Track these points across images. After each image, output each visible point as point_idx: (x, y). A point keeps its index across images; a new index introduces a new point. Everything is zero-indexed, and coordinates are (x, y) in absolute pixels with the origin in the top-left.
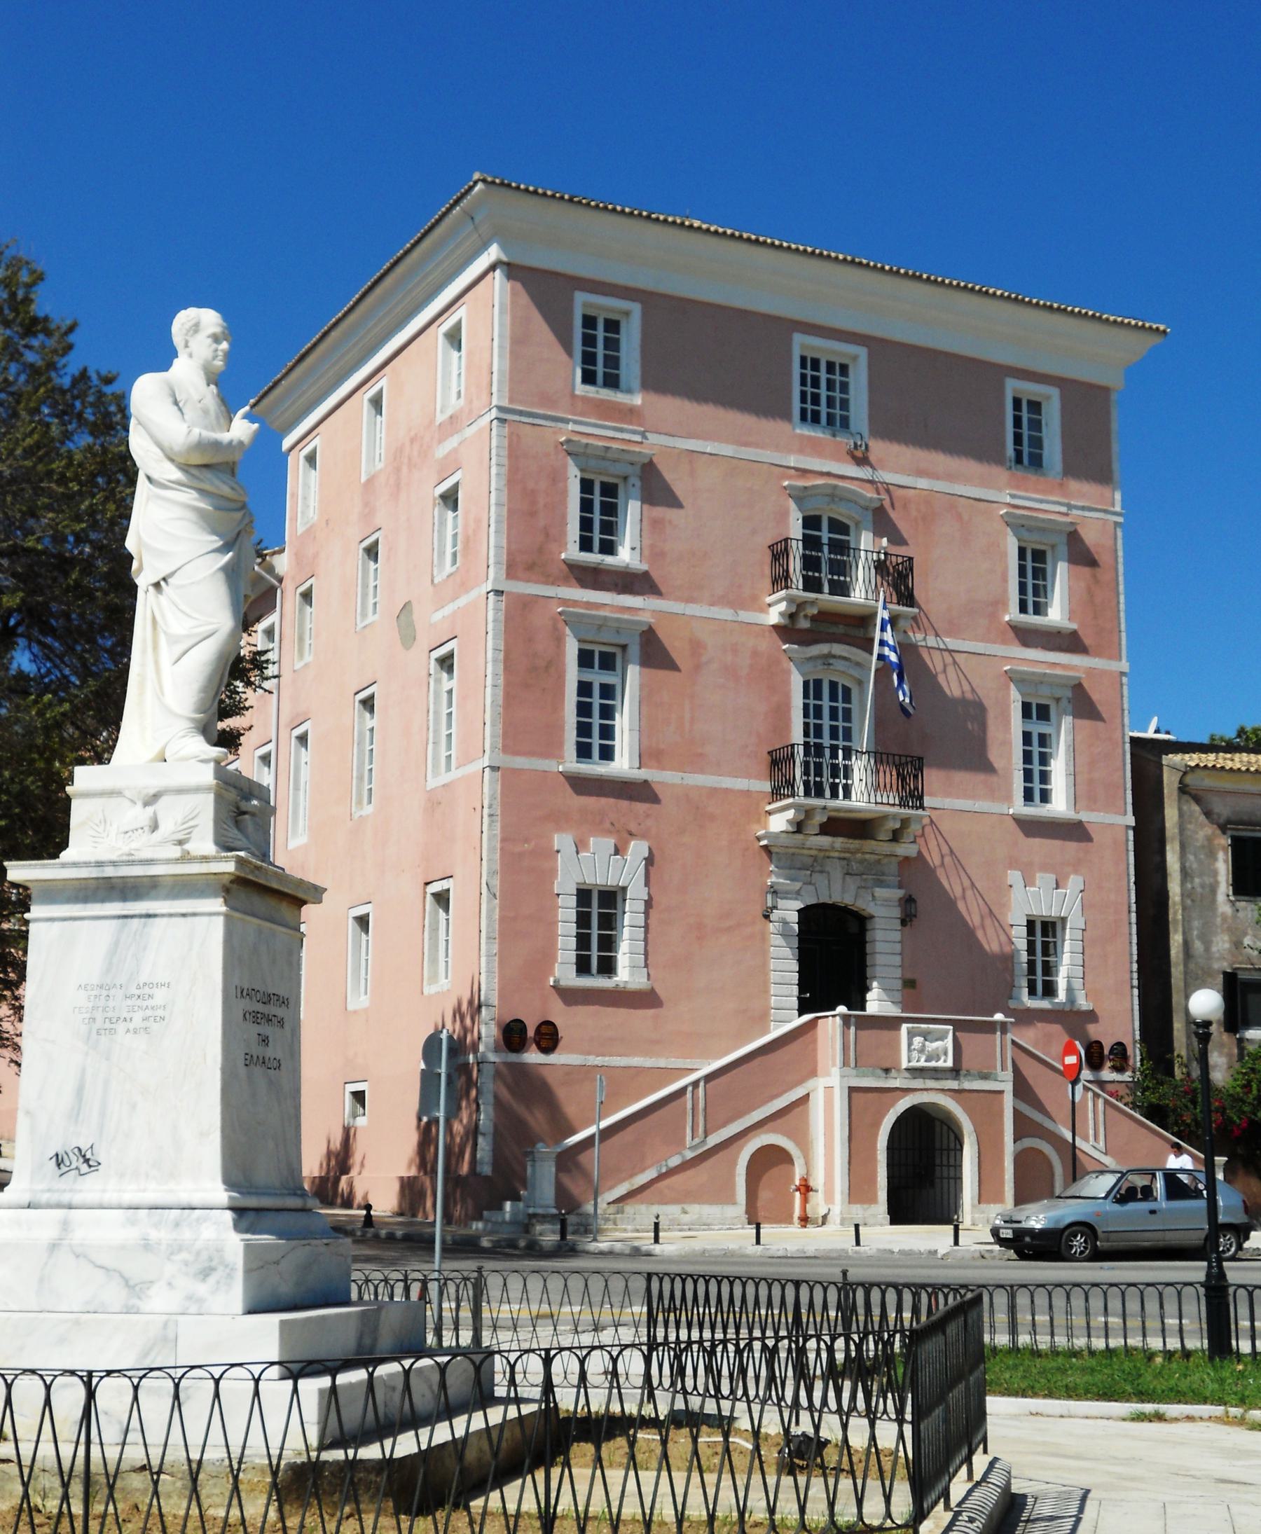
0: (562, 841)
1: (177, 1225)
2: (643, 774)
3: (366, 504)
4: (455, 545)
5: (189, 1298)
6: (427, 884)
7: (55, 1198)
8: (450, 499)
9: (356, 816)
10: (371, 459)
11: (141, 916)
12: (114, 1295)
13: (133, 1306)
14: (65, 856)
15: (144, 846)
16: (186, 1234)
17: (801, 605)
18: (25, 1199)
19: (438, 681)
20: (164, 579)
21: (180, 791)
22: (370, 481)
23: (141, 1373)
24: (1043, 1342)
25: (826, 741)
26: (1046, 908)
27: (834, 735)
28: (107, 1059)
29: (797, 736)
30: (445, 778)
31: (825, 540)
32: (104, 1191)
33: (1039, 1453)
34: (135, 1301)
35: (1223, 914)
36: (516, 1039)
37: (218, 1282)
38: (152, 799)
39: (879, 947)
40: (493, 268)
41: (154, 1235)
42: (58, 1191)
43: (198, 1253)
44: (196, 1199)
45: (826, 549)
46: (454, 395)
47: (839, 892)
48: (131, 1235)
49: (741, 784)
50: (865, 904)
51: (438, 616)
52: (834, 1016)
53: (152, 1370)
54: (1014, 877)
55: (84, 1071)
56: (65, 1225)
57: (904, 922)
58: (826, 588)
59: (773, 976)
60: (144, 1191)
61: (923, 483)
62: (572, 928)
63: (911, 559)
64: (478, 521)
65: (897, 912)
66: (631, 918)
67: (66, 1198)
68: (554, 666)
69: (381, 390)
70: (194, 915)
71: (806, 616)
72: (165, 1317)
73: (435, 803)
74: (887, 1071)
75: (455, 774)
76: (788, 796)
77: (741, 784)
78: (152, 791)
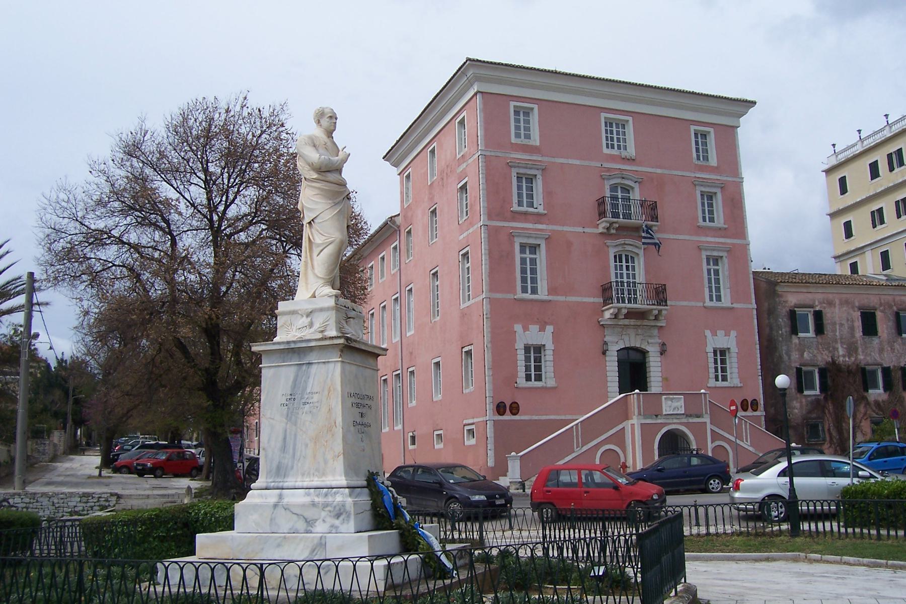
0: (518, 328)
1: (326, 495)
2: (550, 298)
3: (430, 194)
4: (467, 208)
5: (332, 526)
6: (462, 348)
7: (276, 485)
8: (464, 188)
9: (433, 322)
10: (432, 175)
11: (306, 363)
12: (301, 525)
13: (309, 530)
14: (276, 340)
15: (308, 334)
16: (330, 499)
17: (611, 224)
18: (264, 485)
19: (463, 264)
20: (313, 220)
21: (321, 310)
22: (432, 184)
23: (357, 559)
24: (721, 530)
25: (625, 280)
26: (724, 345)
27: (628, 277)
28: (295, 425)
29: (613, 279)
30: (468, 304)
31: (620, 197)
32: (296, 481)
33: (714, 579)
34: (310, 528)
35: (795, 343)
36: (502, 410)
37: (344, 520)
38: (309, 314)
39: (652, 364)
40: (476, 94)
41: (316, 499)
42: (277, 482)
43: (335, 507)
44: (334, 484)
45: (620, 200)
46: (463, 147)
47: (633, 341)
48: (307, 500)
49: (591, 300)
50: (648, 348)
51: (462, 237)
52: (633, 394)
53: (361, 557)
54: (708, 333)
55: (286, 431)
56: (281, 497)
57: (661, 354)
58: (621, 217)
59: (609, 379)
60: (313, 481)
61: (659, 171)
62: (523, 363)
63: (656, 202)
64: (475, 197)
65: (657, 348)
66: (548, 356)
67: (281, 485)
68: (510, 255)
69: (434, 147)
70: (328, 362)
71: (613, 229)
72: (321, 535)
73: (464, 315)
74: (657, 416)
75: (472, 301)
76: (610, 304)
77: (591, 300)
78: (310, 311)
